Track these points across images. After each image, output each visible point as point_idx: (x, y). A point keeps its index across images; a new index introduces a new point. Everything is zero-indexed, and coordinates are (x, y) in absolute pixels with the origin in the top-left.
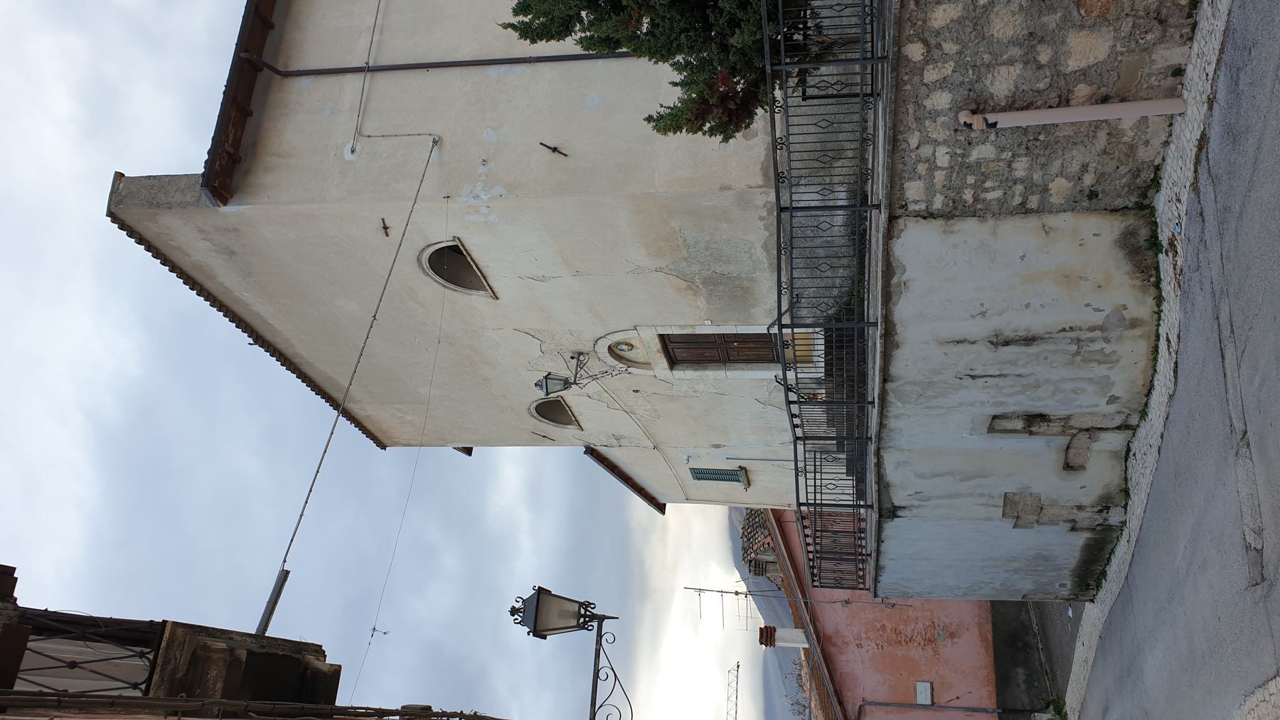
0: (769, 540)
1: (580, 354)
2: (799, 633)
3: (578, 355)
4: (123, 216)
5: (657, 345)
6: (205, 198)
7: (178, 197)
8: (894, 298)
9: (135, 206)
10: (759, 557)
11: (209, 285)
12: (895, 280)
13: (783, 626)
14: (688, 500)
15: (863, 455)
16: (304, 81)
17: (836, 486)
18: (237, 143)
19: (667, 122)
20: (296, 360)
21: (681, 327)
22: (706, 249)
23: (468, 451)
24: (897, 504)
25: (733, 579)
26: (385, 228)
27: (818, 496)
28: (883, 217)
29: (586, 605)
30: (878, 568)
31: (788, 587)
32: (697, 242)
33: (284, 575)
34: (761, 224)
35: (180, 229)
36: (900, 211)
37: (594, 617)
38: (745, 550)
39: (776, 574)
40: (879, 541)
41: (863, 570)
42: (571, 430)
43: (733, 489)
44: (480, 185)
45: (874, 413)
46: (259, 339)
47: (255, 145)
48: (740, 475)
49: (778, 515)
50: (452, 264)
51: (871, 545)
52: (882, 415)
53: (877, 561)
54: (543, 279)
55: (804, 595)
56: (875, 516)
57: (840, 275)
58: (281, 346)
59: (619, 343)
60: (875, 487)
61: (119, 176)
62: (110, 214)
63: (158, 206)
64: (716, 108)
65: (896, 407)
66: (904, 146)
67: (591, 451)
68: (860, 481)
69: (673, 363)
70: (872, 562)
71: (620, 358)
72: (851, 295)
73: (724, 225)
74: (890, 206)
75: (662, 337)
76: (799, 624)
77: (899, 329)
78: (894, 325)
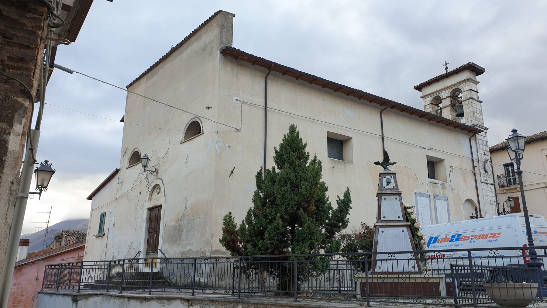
0: (72, 243)
1: (157, 173)
2: (24, 256)
3: (157, 171)
4: (219, 15)
5: (158, 204)
6: (224, 46)
7: (224, 36)
8: (159, 301)
9: (222, 20)
10: (64, 239)
11: (194, 38)
12: (166, 301)
13: (28, 249)
14: (92, 210)
15: (102, 288)
16: (263, 85)
17: (91, 276)
18: (242, 59)
19: (228, 221)
20: (164, 62)
21: (164, 214)
22: (192, 227)
23: (122, 120)
24: (79, 302)
25: (55, 220)
26: (209, 108)
27: (85, 267)
28: (189, 297)
29: (46, 187)
30: (51, 294)
31: (47, 251)
32: (194, 224)
33: (71, 72)
34: (199, 249)
35: (211, 35)
36: (190, 303)
37: (41, 191)
38: (68, 232)
39: (55, 246)
40: (64, 295)
41: (52, 287)
42: (127, 164)
43: (93, 230)
44: (221, 144)
45: (116, 293)
46: (173, 50)
47: (242, 65)
48: (101, 234)
49: (82, 248)
50: (194, 129)
51: (62, 291)
52: (116, 296)
53: (55, 294)
54: (186, 162)
55: (43, 259)
56: (74, 293)
57: (178, 280)
58: (171, 58)
59: (160, 188)
60: (87, 293)
61: (234, 16)
62: (220, 11)
63: (222, 29)
64: (230, 237)
65: (118, 302)
66: (211, 304)
67: (117, 171)
68: (92, 287)
69: (150, 210)
70: (54, 291)
71: (154, 188)
72: (170, 283)
73: (199, 235)
74: (192, 300)
75: (161, 206)
76: (30, 256)
77: (147, 303)
78: (149, 301)
